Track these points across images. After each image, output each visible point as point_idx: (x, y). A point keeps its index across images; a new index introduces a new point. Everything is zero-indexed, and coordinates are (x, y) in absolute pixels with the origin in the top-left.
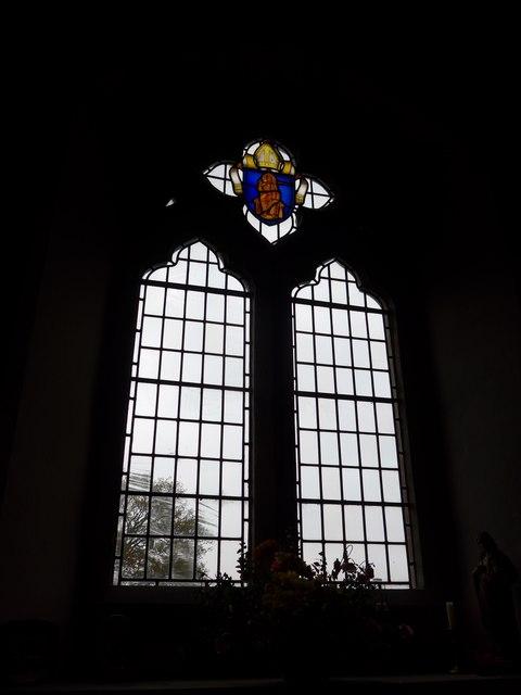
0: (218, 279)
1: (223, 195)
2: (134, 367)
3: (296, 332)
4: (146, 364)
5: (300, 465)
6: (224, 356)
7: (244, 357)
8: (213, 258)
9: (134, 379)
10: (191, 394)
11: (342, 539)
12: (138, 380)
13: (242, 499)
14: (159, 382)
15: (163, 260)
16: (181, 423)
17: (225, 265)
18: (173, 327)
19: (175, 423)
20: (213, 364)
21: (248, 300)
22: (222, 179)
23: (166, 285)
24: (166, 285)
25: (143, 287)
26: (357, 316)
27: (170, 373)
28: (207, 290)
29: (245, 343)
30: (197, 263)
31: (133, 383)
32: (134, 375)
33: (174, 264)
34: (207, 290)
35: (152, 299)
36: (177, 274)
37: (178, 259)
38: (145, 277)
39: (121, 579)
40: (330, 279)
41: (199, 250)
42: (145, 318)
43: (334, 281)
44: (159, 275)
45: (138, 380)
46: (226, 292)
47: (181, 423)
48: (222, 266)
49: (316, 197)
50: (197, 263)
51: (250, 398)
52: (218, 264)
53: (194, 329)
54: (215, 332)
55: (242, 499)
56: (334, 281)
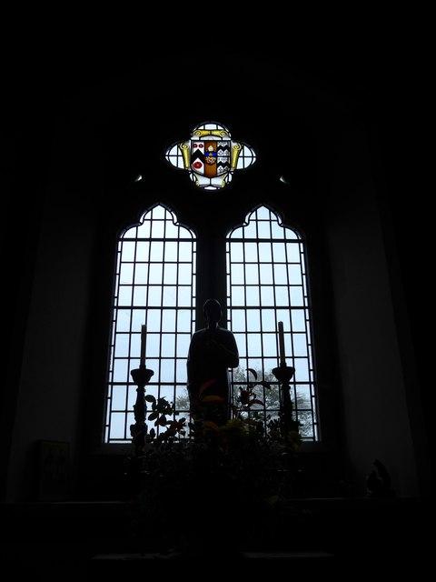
0: (278, 232)
1: (176, 169)
2: (228, 299)
4: (124, 297)
5: (308, 357)
7: (302, 285)
8: (273, 217)
10: (253, 314)
12: (232, 308)
13: (310, 383)
14: (246, 308)
15: (240, 222)
17: (282, 220)
18: (251, 269)
19: (263, 330)
20: (282, 292)
21: (302, 245)
22: (176, 157)
23: (244, 240)
24: (244, 240)
25: (227, 244)
26: (279, 247)
27: (253, 301)
28: (271, 241)
29: (193, 274)
30: (159, 221)
33: (247, 224)
34: (271, 241)
35: (127, 250)
36: (250, 232)
38: (228, 237)
39: (109, 439)
40: (257, 220)
41: (263, 212)
43: (263, 221)
44: (237, 234)
45: (232, 308)
46: (285, 241)
48: (280, 222)
49: (246, 158)
50: (159, 221)
52: (278, 221)
53: (266, 269)
54: (280, 269)
55: (310, 383)
56: (263, 221)
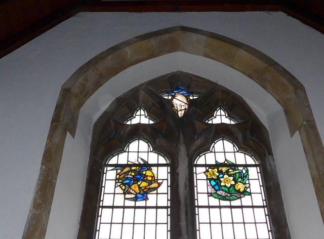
3: (266, 223)
6: (221, 223)
9: (197, 206)
11: (121, 225)
12: (199, 207)
16: (132, 225)
19: (211, 222)
23: (242, 207)
31: (197, 208)
32: (169, 209)
33: (215, 117)
37: (136, 115)
42: (200, 224)
45: (199, 207)
47: (132, 225)
51: (269, 219)
